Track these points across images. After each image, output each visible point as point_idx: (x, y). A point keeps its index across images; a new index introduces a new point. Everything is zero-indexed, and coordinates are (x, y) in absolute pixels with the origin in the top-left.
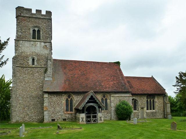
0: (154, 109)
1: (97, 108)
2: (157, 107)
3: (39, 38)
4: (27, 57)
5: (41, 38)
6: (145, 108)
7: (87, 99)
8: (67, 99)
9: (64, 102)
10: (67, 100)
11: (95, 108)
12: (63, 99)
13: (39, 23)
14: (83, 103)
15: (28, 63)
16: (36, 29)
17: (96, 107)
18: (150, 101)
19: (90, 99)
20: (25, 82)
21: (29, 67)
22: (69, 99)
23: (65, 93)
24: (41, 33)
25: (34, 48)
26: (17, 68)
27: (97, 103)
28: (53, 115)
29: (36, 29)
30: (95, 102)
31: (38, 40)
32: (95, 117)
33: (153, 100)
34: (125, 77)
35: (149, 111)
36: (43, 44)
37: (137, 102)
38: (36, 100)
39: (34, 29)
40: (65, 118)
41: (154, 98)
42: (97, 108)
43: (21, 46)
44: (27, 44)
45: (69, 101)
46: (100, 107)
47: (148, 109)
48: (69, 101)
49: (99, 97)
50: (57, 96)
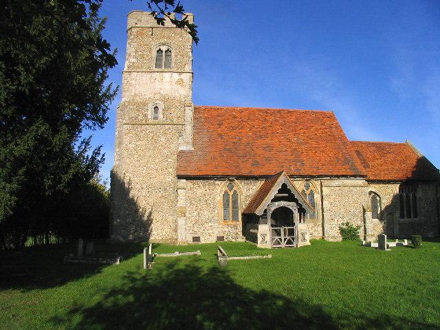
0: (416, 216)
1: (296, 215)
2: (422, 210)
3: (168, 65)
4: (145, 104)
5: (173, 65)
6: (397, 214)
7: (274, 192)
8: (226, 192)
9: (219, 198)
10: (226, 195)
11: (292, 213)
12: (220, 187)
13: (169, 37)
14: (264, 202)
15: (146, 116)
16: (164, 48)
17: (294, 211)
18: (408, 196)
19: (280, 191)
20: (139, 156)
21: (147, 124)
22: (231, 193)
23: (222, 178)
24: (173, 54)
25: (161, 89)
26: (125, 126)
27: (296, 201)
28: (195, 229)
29: (164, 48)
30: (291, 198)
31: (166, 70)
32: (291, 232)
33: (414, 196)
34: (353, 143)
35: (406, 220)
36: (176, 76)
37: (378, 198)
38: (160, 195)
39: (160, 49)
40: (222, 235)
41: (416, 191)
42: (296, 215)
43: (133, 82)
44: (146, 77)
45: (231, 197)
46: (302, 211)
47: (402, 216)
48: (231, 197)
49: (298, 185)
50: (204, 186)
